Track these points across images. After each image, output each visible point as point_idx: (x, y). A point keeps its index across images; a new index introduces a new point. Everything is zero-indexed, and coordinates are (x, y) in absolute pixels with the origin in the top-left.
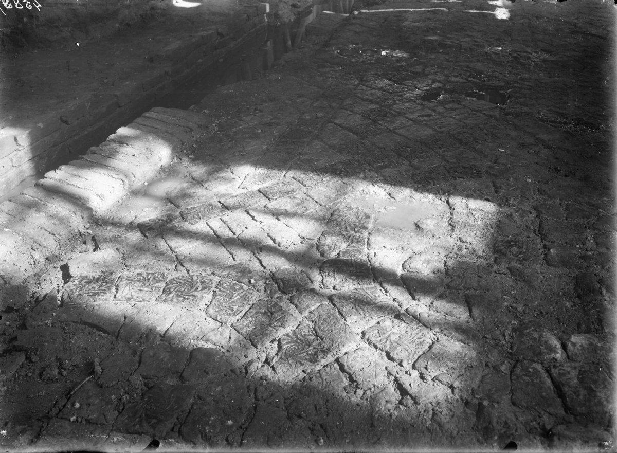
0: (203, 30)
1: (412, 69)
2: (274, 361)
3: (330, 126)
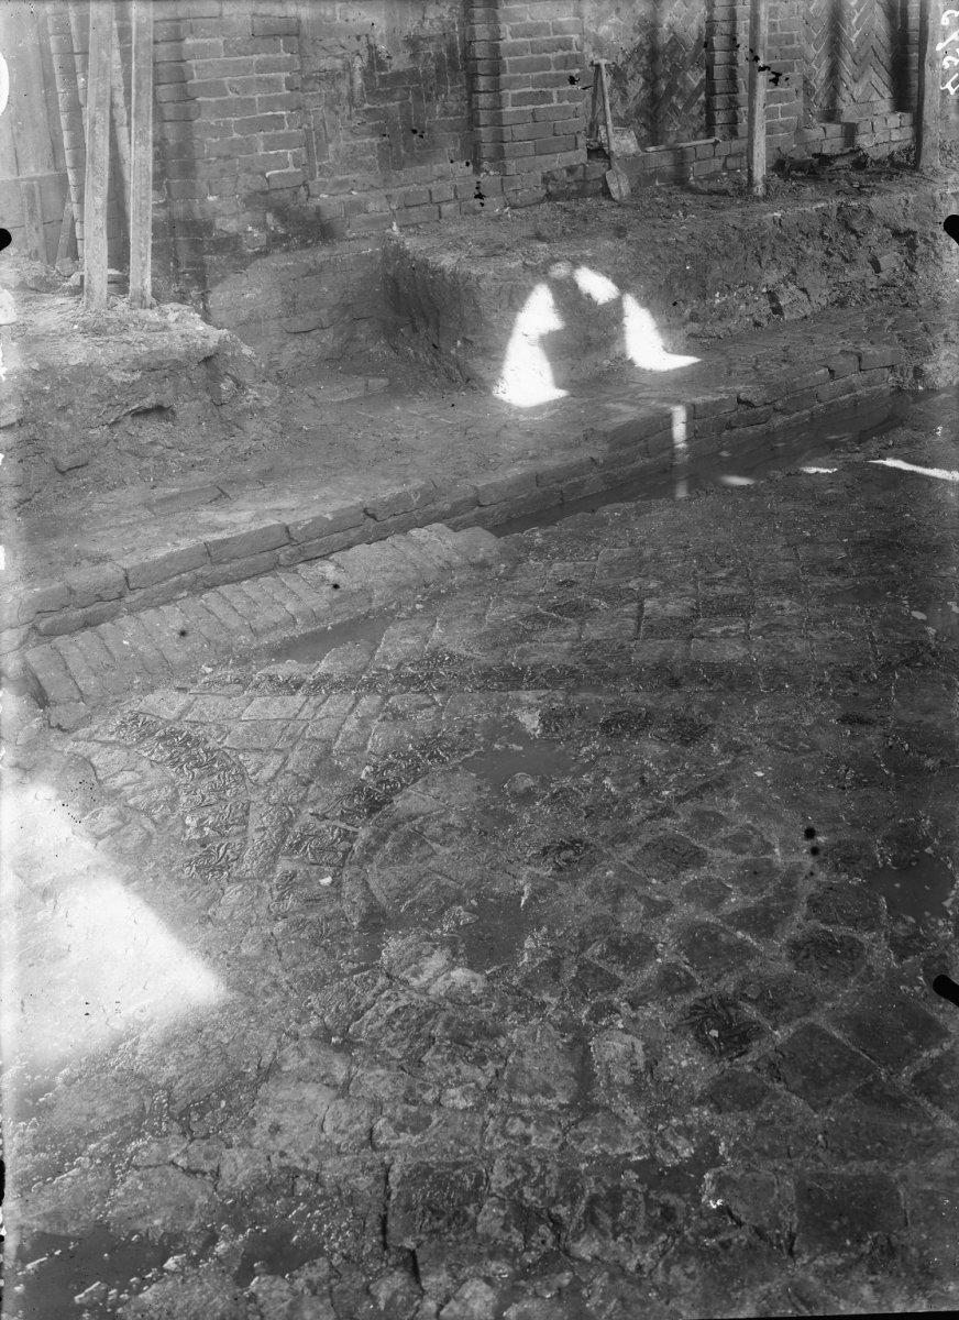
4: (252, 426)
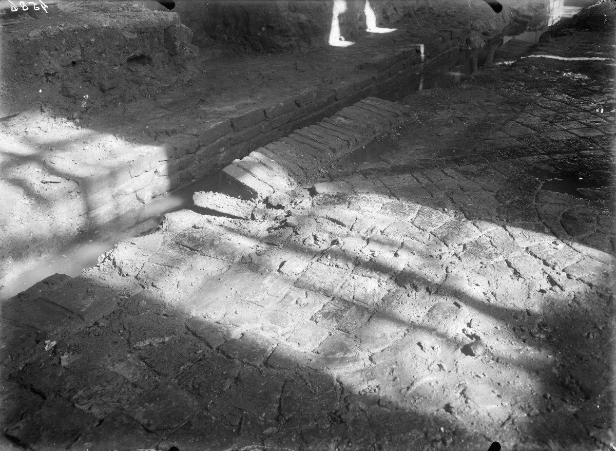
0: (404, 47)
1: (591, 88)
2: (460, 254)
3: (513, 123)
4: (190, 66)
